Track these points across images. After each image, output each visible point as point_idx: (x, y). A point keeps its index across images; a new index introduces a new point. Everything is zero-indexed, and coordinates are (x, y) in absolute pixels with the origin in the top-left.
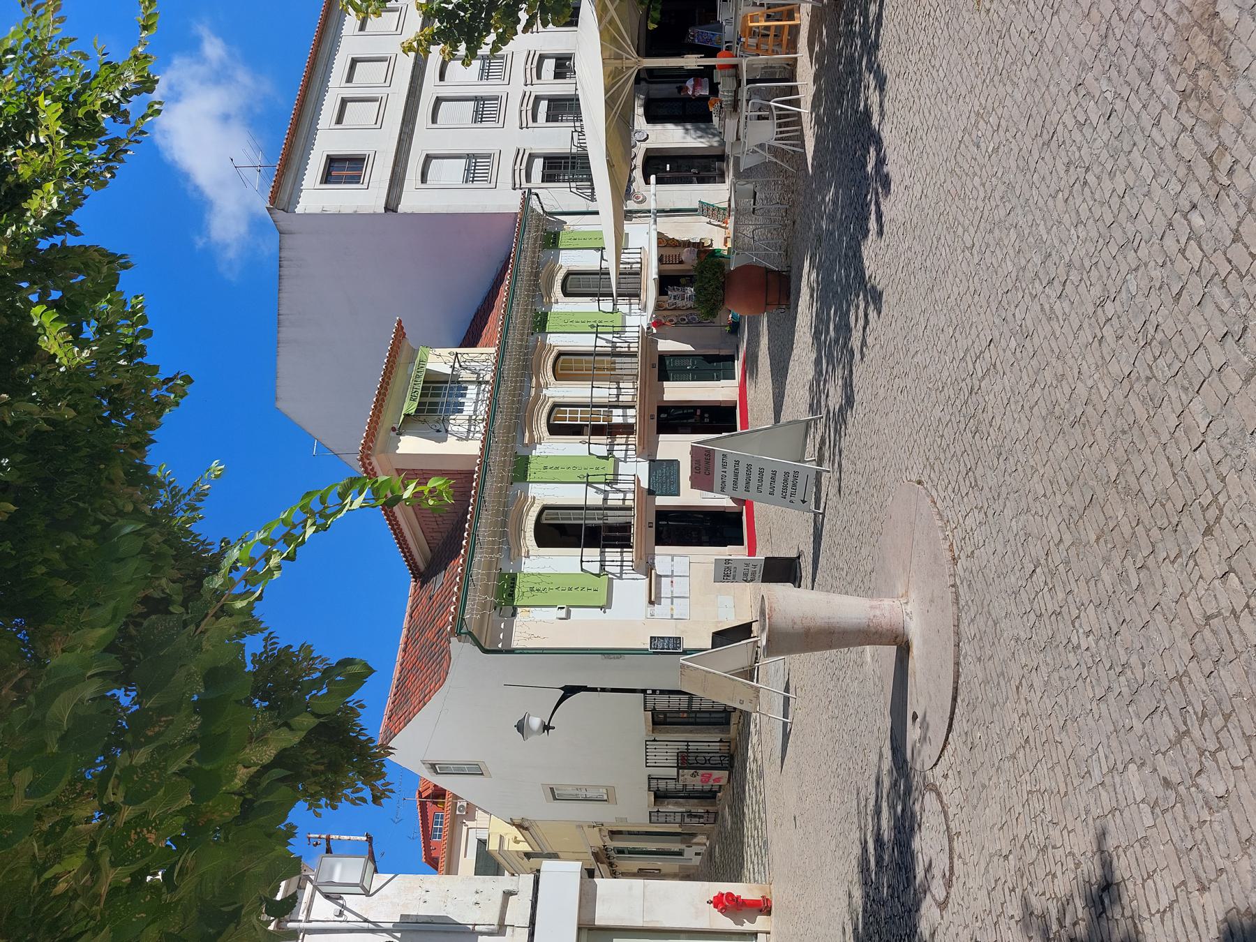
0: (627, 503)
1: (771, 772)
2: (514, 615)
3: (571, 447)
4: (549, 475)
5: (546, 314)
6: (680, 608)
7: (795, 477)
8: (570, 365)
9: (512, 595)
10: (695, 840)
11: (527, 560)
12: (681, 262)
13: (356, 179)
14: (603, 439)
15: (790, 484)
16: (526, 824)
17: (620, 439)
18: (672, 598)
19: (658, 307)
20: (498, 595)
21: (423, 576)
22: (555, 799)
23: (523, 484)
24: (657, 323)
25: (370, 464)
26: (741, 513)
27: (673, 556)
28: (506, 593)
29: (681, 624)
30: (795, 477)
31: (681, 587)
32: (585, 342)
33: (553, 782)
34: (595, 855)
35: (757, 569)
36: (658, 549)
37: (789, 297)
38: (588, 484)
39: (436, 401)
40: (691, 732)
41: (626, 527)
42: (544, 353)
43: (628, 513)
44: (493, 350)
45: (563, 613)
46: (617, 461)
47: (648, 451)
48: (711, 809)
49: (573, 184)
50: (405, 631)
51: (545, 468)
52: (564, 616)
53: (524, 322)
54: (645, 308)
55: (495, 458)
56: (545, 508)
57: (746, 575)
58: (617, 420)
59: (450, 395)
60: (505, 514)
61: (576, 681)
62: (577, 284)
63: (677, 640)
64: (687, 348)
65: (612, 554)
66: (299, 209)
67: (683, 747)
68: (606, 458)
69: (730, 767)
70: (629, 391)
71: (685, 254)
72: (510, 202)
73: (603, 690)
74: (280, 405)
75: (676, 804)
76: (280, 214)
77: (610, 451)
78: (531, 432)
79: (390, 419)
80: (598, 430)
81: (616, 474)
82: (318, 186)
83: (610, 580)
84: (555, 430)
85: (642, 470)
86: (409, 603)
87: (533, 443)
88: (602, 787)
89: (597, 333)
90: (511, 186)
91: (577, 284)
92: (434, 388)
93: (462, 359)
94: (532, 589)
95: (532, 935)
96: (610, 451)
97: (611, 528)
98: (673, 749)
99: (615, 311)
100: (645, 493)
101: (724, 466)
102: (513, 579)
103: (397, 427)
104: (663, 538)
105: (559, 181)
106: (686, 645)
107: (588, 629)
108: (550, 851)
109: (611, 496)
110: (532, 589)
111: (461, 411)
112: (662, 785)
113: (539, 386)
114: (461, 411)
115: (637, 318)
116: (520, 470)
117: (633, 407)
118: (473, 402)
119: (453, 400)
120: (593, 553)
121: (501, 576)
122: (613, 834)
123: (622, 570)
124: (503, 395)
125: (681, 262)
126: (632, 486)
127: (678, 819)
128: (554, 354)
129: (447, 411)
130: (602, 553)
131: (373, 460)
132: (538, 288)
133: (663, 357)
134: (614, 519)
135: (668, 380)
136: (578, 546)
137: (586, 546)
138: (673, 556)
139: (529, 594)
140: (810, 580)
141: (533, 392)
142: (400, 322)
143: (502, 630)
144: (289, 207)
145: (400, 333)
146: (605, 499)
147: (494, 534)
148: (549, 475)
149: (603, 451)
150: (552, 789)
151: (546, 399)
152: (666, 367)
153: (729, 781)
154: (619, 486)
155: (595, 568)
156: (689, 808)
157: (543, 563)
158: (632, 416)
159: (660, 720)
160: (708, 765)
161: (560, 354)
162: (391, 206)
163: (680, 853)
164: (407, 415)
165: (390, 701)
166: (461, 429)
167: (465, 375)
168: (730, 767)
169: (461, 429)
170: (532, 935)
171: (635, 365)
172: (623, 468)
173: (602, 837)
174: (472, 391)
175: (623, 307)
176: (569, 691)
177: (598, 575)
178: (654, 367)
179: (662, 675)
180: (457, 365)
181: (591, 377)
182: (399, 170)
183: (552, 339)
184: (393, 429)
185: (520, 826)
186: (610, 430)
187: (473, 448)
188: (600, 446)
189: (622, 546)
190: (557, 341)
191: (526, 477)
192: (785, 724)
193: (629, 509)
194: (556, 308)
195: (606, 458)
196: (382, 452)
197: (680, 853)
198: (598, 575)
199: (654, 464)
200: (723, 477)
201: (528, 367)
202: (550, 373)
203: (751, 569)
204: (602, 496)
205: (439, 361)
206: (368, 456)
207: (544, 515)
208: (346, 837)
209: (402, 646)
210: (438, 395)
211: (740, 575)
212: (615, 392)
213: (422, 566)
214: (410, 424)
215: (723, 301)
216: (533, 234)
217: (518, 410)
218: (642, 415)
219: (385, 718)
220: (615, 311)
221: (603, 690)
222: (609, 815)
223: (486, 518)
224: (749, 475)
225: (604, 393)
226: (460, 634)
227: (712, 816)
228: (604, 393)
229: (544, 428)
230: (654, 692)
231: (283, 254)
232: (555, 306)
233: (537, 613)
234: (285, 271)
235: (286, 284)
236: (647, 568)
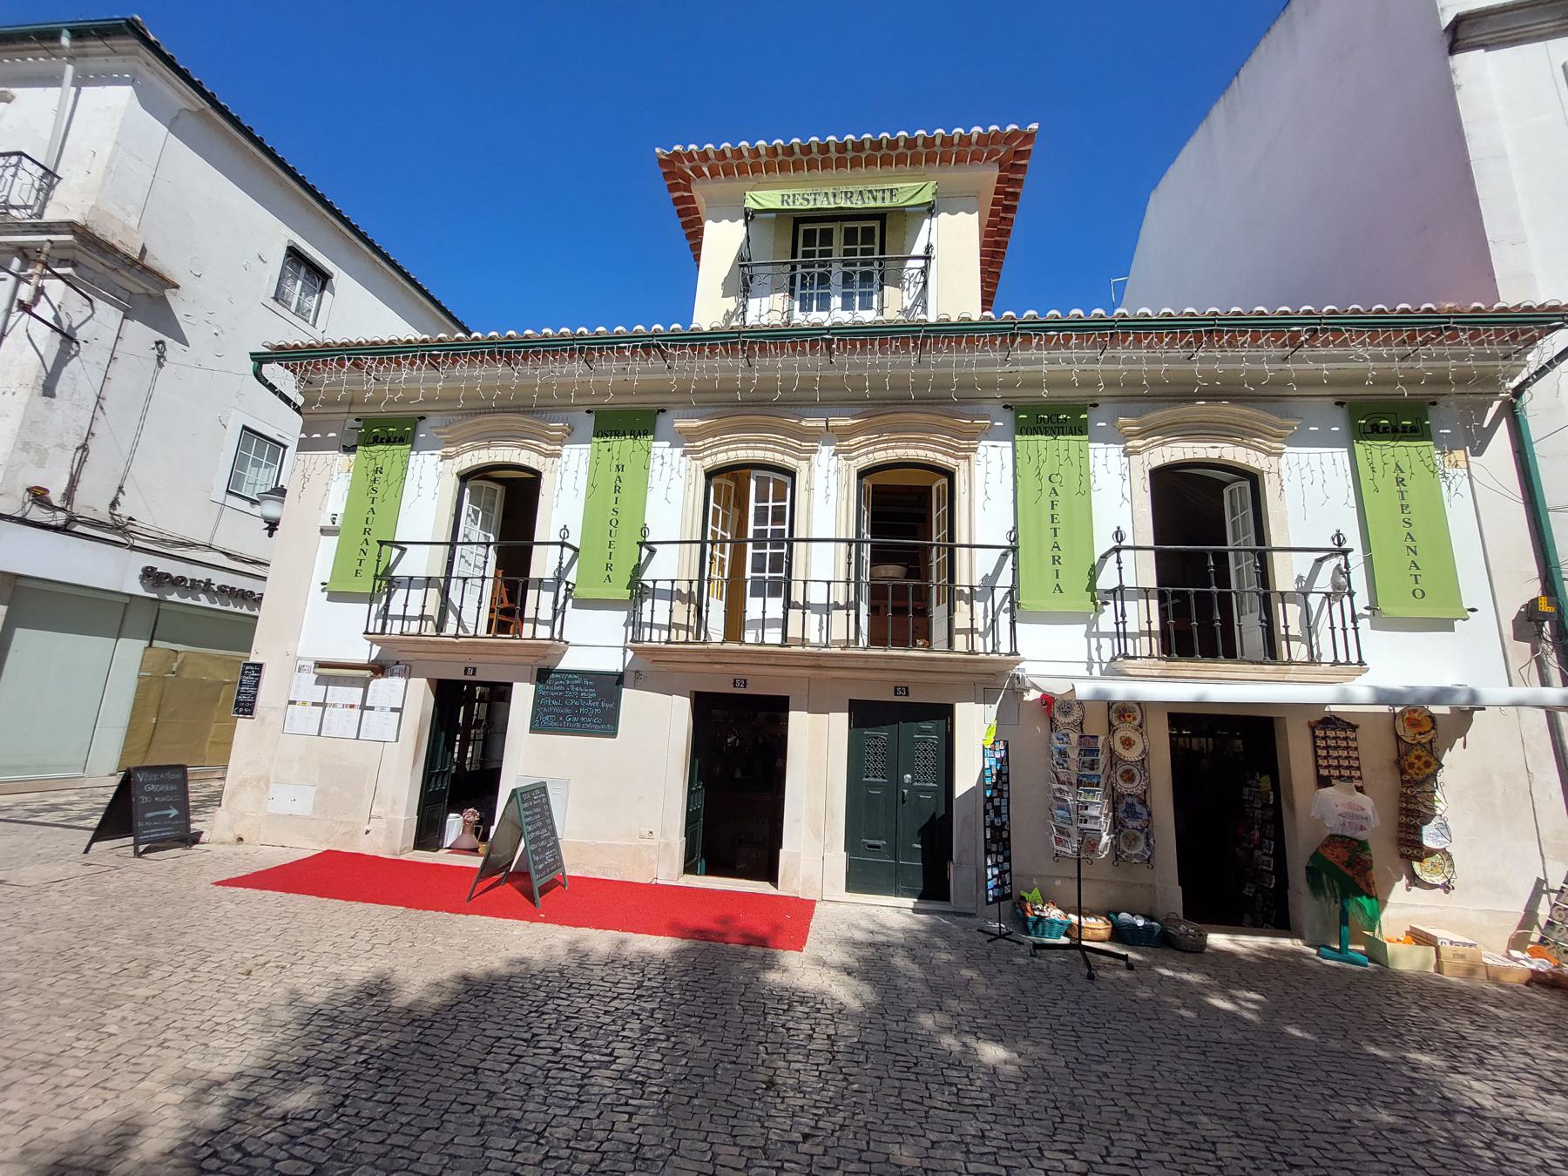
0: (960, 642)
2: (349, 449)
9: (377, 440)
11: (436, 458)
18: (324, 705)
19: (1122, 711)
23: (1011, 428)
31: (341, 721)
42: (944, 438)
47: (651, 668)
54: (1112, 672)
58: (753, 608)
65: (1143, 615)
74: (127, 91)
84: (728, 483)
95: (10, 518)
100: (545, 663)
113: (845, 434)
120: (1142, 570)
130: (1145, 593)
136: (1160, 536)
137: (1161, 558)
139: (371, 467)
146: (540, 584)
170: (10, 518)
177: (1091, 587)
193: (950, 643)
202: (880, 457)
232: (1115, 451)
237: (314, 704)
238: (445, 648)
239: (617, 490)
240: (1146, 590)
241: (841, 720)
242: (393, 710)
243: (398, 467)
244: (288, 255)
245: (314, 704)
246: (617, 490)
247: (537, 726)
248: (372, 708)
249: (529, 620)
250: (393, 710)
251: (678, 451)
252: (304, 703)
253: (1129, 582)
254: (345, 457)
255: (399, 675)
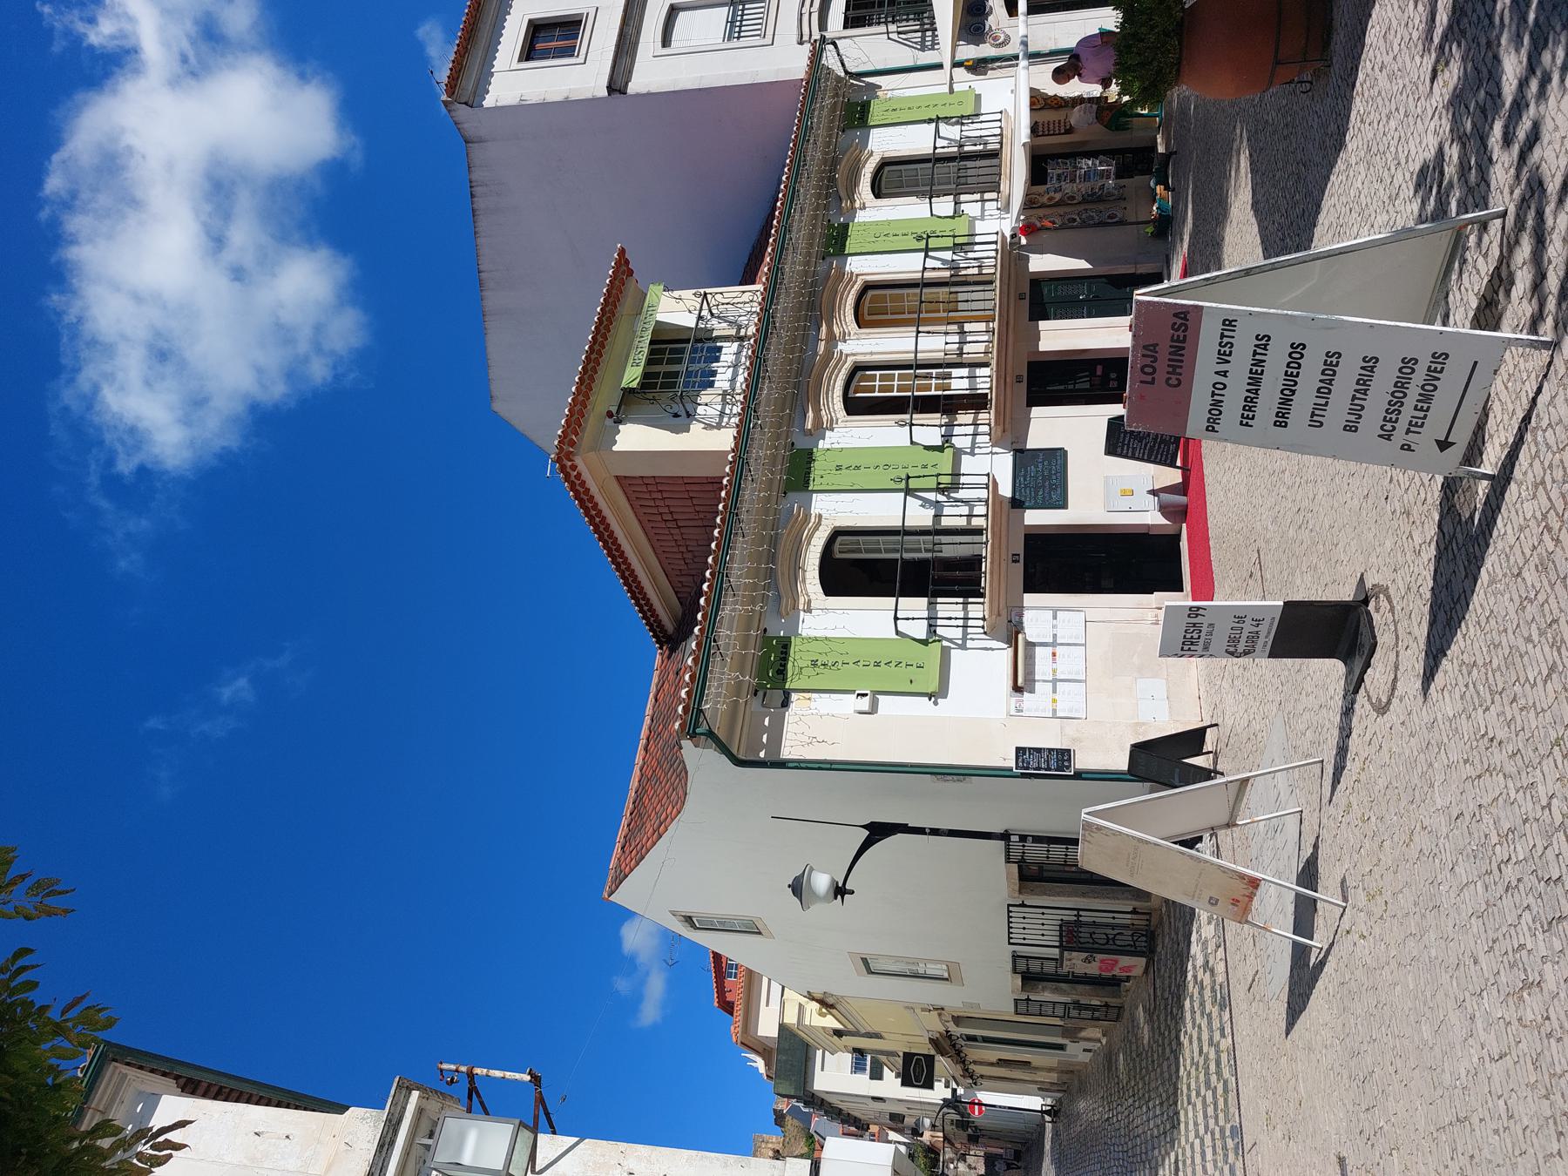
0: (976, 522)
1: (1257, 1013)
2: (786, 704)
3: (884, 433)
4: (845, 479)
5: (845, 227)
6: (1070, 699)
7: (1434, 373)
8: (881, 301)
9: (782, 672)
10: (1083, 1034)
12: (1070, 131)
13: (568, 52)
14: (936, 418)
15: (1413, 393)
16: (830, 1001)
17: (965, 418)
18: (1055, 682)
19: (1029, 203)
20: (761, 673)
21: (671, 640)
22: (870, 972)
24: (1028, 229)
25: (574, 467)
26: (1178, 537)
27: (1055, 611)
28: (773, 672)
29: (1071, 729)
30: (1434, 373)
31: (1070, 662)
32: (908, 265)
33: (867, 950)
34: (934, 1042)
35: (1263, 629)
36: (1029, 599)
37: (1326, 43)
38: (908, 492)
39: (675, 368)
40: (1084, 895)
41: (974, 562)
42: (841, 287)
43: (976, 538)
44: (759, 287)
45: (864, 703)
46: (958, 454)
47: (1011, 435)
48: (1113, 1001)
49: (892, 28)
50: (647, 720)
51: (839, 468)
52: (866, 708)
53: (812, 236)
54: (1007, 208)
55: (759, 452)
56: (837, 533)
57: (1234, 641)
59: (692, 360)
60: (774, 541)
61: (891, 813)
62: (895, 177)
63: (1064, 755)
64: (1081, 264)
65: (949, 608)
66: (489, 102)
67: (1070, 916)
68: (940, 449)
69: (1149, 952)
70: (980, 338)
71: (1076, 116)
72: (789, 62)
73: (935, 832)
75: (1056, 991)
76: (462, 112)
77: (947, 437)
78: (817, 411)
79: (604, 398)
80: (927, 405)
81: (956, 474)
82: (515, 65)
83: (945, 653)
84: (855, 407)
85: (1002, 466)
86: (655, 680)
87: (820, 430)
88: (941, 962)
89: (927, 250)
90: (795, 38)
91: (895, 177)
92: (672, 351)
93: (713, 302)
94: (814, 663)
96: (947, 437)
97: (950, 564)
98: (1054, 918)
99: (957, 214)
100: (1006, 506)
101: (1224, 357)
102: (785, 646)
103: (614, 409)
104: (1037, 582)
105: (870, 25)
106: (1082, 762)
107: (905, 730)
108: (869, 1029)
109: (946, 511)
110: (814, 663)
111: (711, 384)
112: (1035, 966)
114: (711, 384)
115: (994, 220)
116: (798, 472)
117: (986, 365)
118: (729, 369)
119: (695, 367)
120: (915, 606)
121: (766, 639)
122: (957, 1020)
123: (965, 634)
124: (774, 355)
125: (1070, 131)
126: (983, 494)
127: (1060, 1011)
128: (857, 287)
129: (686, 384)
130: (932, 605)
131: (578, 461)
132: (835, 190)
133: (1039, 282)
134: (953, 549)
135: (1048, 319)
138: (1055, 611)
139: (810, 671)
140: (1413, 660)
141: (822, 347)
142: (622, 252)
143: (765, 730)
144: (474, 101)
145: (623, 269)
146: (937, 516)
147: (754, 573)
148: (845, 479)
149: (933, 436)
150: (865, 961)
151: (843, 357)
152: (1048, 297)
153: (1146, 971)
154: (962, 494)
155: (919, 630)
156: (1076, 997)
157: (832, 620)
158: (985, 380)
159: (1032, 876)
160: (1112, 947)
161: (868, 287)
162: (617, 86)
163: (1061, 1047)
164: (628, 392)
165: (624, 822)
166: (710, 411)
167: (720, 329)
168: (1149, 952)
169: (710, 411)
171: (992, 297)
172: (967, 464)
173: (944, 1022)
174: (729, 351)
175: (971, 208)
176: (878, 831)
178: (1019, 380)
179: (1036, 810)
180: (705, 313)
181: (917, 320)
182: (630, 30)
183: (855, 265)
184: (610, 414)
185: (822, 1002)
186: (948, 405)
187: (724, 440)
188: (929, 430)
189: (966, 594)
190: (862, 267)
191: (807, 483)
192: (1300, 953)
193: (978, 531)
194: (861, 217)
195: (940, 449)
196: (593, 449)
197: (1061, 1047)
198: (925, 642)
199: (1023, 458)
200: (1218, 388)
201: (815, 308)
203: (1248, 627)
204: (932, 512)
205: (675, 309)
206: (569, 456)
207: (837, 547)
208: (498, 1074)
209: (643, 742)
210: (679, 361)
211: (1220, 641)
212: (956, 338)
213: (669, 626)
214: (631, 404)
215: (1178, 64)
216: (828, 101)
217: (799, 373)
218: (1001, 376)
219: (618, 846)
220: (957, 214)
221: (935, 832)
222: (953, 998)
223: (742, 548)
224: (1291, 377)
225: (934, 344)
226: (693, 736)
227: (1113, 1013)
228: (934, 344)
229: (838, 404)
230: (1023, 838)
231: (474, 177)
233: (823, 702)
234: (480, 203)
235: (483, 224)
236: (1010, 630)
237: (1054, 691)
238: (995, 584)
239: (858, 468)
240: (930, 603)
241: (1043, 325)
242: (1055, 617)
243: (814, 646)
244: (546, 55)
245: (1054, 691)
246: (858, 468)
247: (1063, 505)
248: (1055, 636)
249: (969, 522)
250: (1055, 617)
251: (828, 433)
252: (1054, 701)
253: (925, 614)
254: (793, 706)
255: (1021, 616)
